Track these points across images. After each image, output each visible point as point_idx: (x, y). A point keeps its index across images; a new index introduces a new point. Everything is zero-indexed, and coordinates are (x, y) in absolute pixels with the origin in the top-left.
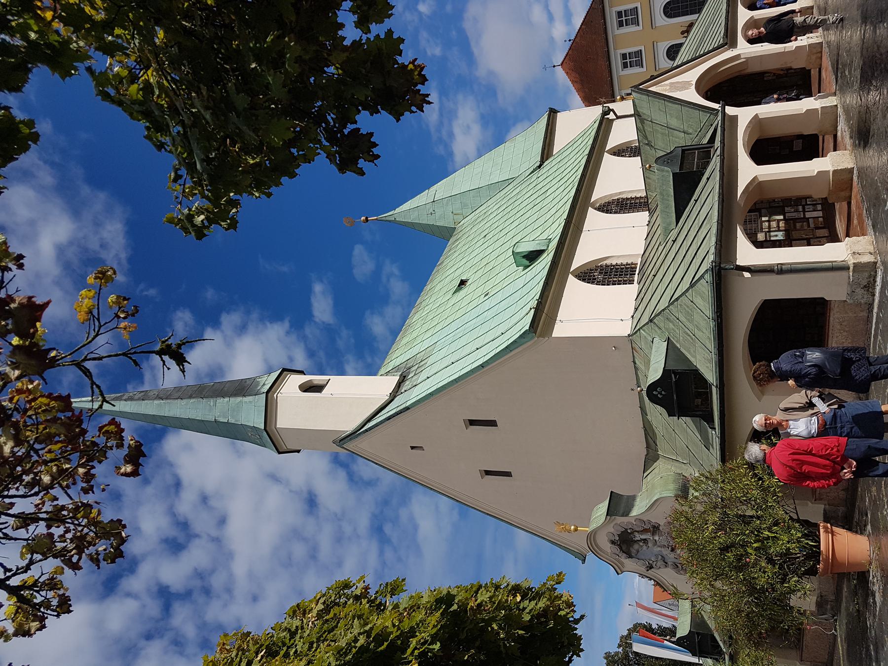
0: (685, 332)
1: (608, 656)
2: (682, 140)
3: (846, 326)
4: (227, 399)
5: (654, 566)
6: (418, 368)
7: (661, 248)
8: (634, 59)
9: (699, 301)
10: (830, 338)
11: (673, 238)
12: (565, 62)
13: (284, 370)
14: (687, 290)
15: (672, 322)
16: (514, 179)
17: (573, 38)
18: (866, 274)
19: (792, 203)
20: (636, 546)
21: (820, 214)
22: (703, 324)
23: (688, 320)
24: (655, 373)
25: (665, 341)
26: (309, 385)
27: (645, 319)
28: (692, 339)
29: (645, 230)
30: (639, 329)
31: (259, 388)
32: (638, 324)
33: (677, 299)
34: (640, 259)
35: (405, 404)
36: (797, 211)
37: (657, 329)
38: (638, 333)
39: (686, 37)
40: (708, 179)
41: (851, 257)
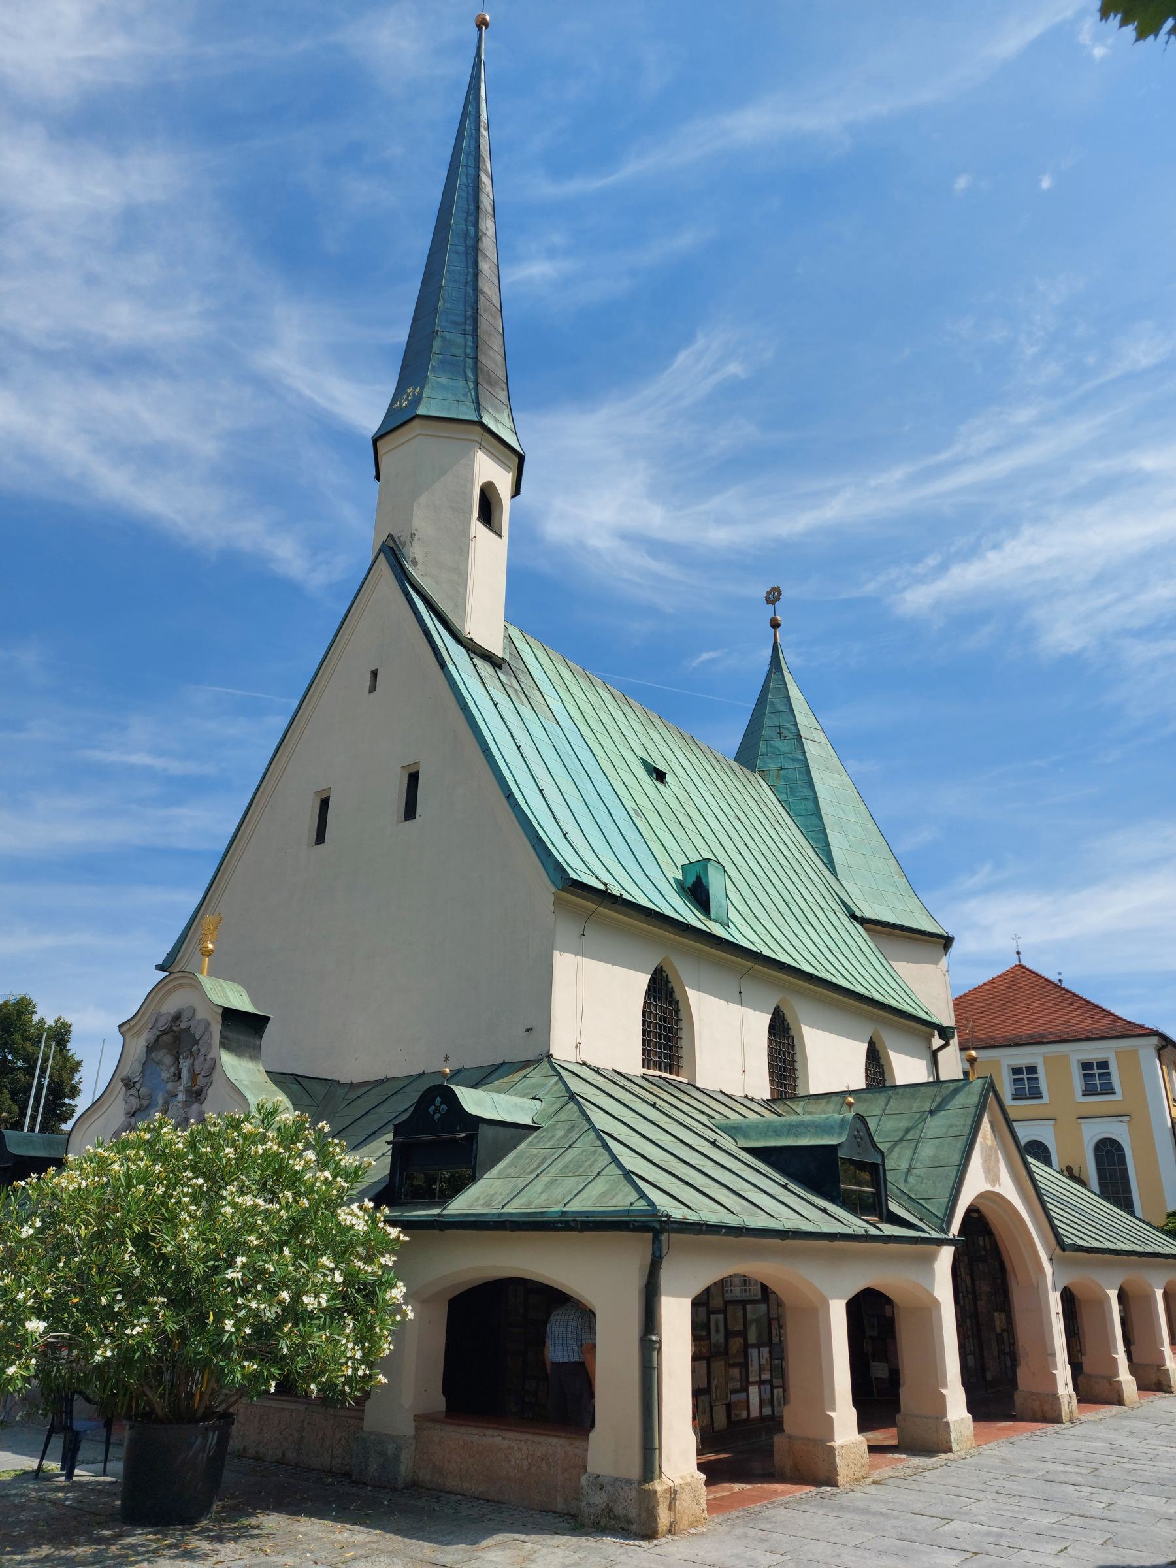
0: (545, 1159)
1: (23, 1007)
2: (896, 1163)
3: (540, 1468)
5: (133, 1091)
6: (516, 690)
7: (704, 1119)
8: (1027, 1086)
9: (599, 1186)
10: (519, 1436)
11: (721, 1141)
12: (1025, 971)
13: (521, 458)
14: (620, 1166)
15: (566, 1136)
16: (834, 872)
17: (1064, 985)
18: (633, 1513)
19: (776, 1361)
20: (168, 1060)
21: (755, 1412)
22: (557, 1192)
23: (566, 1167)
24: (474, 1101)
25: (533, 1121)
26: (493, 501)
27: (575, 1085)
28: (532, 1172)
29: (738, 1092)
30: (559, 1074)
31: (490, 411)
32: (569, 1074)
33: (606, 1146)
34: (685, 1080)
35: (450, 661)
36: (761, 1370)
37: (557, 1106)
38: (553, 1073)
39: (1062, 1171)
40: (824, 1211)
41: (666, 1487)
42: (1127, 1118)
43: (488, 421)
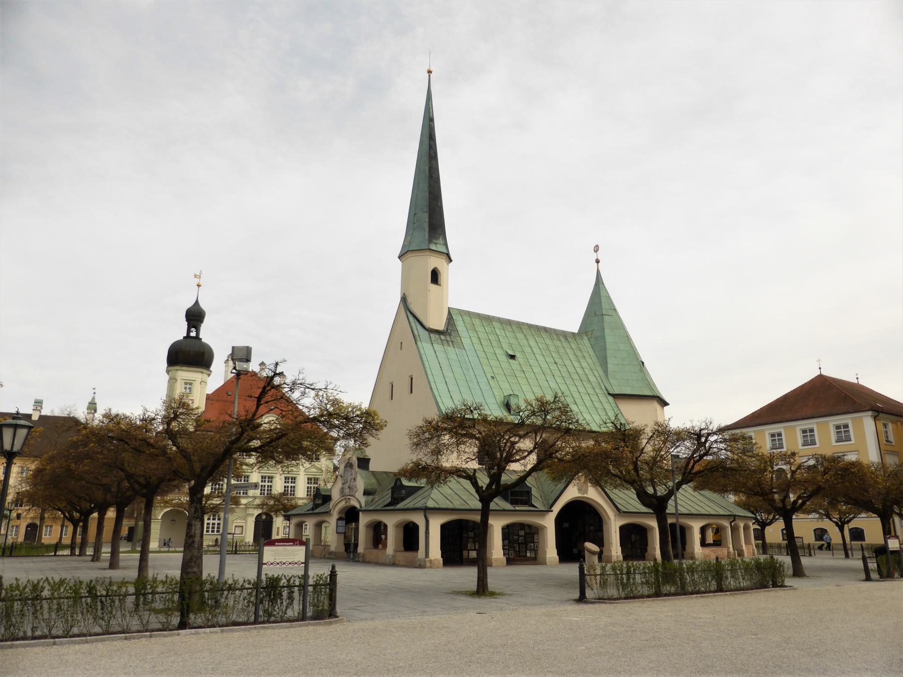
4: (427, 220)
42: (857, 452)
43: (430, 248)
